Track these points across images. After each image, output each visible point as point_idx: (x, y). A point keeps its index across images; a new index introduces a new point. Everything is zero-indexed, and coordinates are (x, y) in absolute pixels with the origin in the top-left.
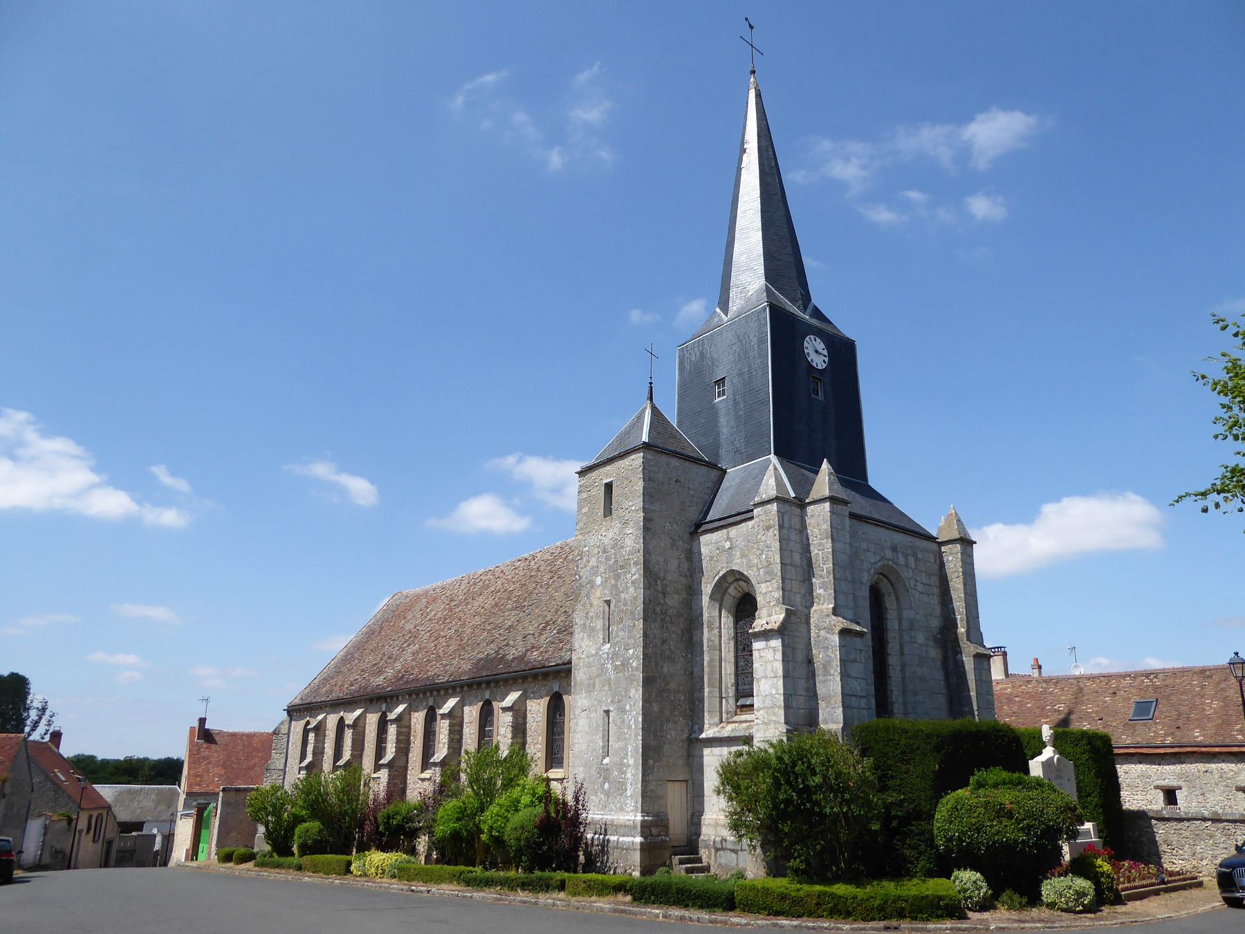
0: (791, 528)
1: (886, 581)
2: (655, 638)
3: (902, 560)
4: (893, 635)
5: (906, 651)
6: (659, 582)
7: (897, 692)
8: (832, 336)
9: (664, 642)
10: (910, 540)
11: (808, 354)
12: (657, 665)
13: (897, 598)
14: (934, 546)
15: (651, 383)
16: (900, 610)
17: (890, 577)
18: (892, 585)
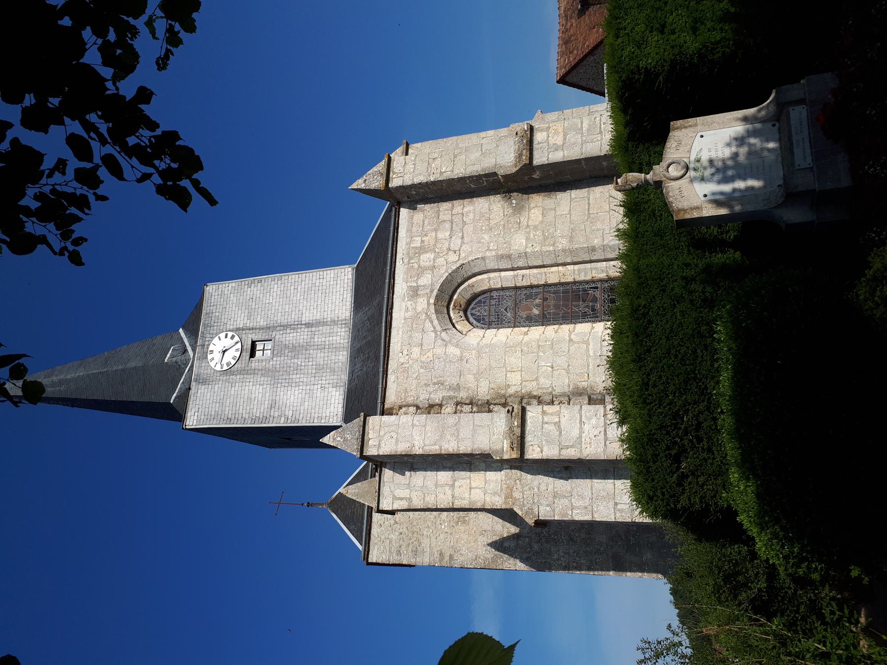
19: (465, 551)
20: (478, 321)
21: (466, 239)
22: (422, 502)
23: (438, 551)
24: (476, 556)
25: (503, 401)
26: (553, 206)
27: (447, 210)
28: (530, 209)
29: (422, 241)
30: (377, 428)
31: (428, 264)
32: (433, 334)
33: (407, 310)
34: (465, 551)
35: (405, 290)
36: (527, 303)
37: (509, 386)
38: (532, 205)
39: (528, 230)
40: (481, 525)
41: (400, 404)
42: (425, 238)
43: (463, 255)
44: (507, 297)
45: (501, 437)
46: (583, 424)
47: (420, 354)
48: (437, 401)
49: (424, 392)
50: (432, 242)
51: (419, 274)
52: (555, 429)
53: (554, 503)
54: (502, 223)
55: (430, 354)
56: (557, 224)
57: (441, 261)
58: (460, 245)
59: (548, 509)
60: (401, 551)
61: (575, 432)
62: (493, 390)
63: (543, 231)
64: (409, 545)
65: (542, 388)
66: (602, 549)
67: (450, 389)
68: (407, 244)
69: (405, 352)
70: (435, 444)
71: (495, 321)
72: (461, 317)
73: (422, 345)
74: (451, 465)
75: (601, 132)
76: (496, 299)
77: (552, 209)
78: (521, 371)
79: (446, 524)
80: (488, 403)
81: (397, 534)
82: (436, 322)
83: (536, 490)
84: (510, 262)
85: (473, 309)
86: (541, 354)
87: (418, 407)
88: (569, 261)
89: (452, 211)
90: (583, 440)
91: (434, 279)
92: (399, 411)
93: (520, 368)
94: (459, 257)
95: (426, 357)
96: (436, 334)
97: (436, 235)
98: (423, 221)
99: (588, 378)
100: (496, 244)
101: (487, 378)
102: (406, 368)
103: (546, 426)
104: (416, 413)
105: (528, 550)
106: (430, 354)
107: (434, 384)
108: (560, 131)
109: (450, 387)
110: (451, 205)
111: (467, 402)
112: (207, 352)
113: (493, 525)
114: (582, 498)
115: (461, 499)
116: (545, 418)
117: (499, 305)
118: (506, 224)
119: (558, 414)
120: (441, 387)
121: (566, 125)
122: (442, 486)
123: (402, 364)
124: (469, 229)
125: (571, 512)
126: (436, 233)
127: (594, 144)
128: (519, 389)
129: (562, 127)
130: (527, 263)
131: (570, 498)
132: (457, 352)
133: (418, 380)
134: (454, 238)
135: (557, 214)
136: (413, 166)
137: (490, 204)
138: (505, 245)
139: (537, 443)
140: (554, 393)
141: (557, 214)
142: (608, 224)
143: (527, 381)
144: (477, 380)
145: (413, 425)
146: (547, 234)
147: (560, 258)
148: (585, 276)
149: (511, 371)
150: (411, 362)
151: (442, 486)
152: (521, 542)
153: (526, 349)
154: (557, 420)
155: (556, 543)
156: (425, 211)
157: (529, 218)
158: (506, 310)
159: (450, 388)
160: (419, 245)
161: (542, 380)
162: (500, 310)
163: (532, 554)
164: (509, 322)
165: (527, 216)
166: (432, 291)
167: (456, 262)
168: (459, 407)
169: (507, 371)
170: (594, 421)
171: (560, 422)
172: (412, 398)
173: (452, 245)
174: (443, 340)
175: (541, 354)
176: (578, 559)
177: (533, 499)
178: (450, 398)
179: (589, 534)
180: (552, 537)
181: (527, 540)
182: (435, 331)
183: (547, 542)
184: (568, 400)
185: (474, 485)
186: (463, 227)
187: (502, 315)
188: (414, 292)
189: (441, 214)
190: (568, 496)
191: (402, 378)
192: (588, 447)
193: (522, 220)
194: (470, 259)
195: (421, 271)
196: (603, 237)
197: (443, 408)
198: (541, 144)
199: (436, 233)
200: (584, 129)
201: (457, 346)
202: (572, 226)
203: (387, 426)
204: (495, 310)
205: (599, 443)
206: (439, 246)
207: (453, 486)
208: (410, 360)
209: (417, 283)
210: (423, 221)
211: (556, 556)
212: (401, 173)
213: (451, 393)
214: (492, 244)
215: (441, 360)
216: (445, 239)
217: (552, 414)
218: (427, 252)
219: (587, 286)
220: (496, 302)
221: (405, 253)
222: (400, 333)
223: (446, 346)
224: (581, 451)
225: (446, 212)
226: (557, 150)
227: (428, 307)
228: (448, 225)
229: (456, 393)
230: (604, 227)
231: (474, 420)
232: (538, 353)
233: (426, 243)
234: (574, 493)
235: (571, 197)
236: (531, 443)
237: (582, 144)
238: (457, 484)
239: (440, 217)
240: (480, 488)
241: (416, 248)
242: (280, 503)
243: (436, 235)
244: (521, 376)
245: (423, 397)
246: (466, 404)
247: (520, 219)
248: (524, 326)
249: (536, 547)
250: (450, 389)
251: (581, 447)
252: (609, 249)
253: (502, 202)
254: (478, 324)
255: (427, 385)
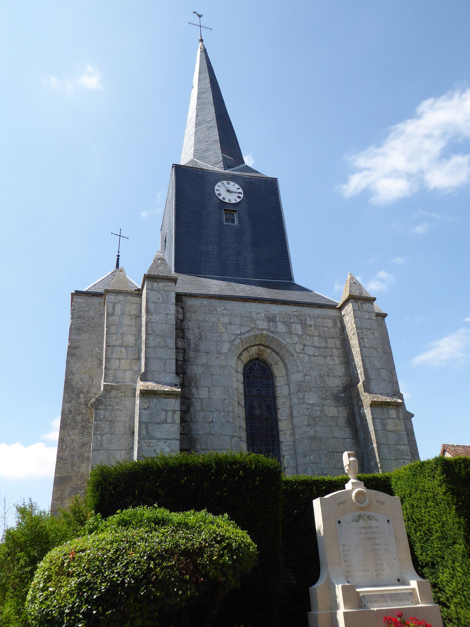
0: (124, 314)
1: (268, 351)
2: (73, 442)
3: (281, 328)
4: (283, 400)
5: (295, 414)
6: (82, 396)
7: (288, 457)
8: (250, 178)
9: (83, 445)
10: (294, 310)
11: (224, 198)
12: (73, 465)
13: (285, 365)
14: (333, 313)
15: (118, 256)
16: (287, 375)
17: (271, 346)
18: (278, 354)
19: (78, 365)
20: (250, 369)
21: (313, 359)
22: (111, 324)
23: (79, 345)
24: (74, 373)
25: (186, 384)
26: (339, 424)
27: (335, 344)
28: (336, 407)
29: (311, 325)
30: (166, 289)
31: (293, 329)
32: (239, 333)
33: (258, 314)
34: (78, 365)
35: (273, 312)
36: (264, 406)
37: (198, 389)
38: (339, 408)
39: (320, 405)
40: (97, 377)
41: (185, 308)
42: (313, 328)
43: (301, 356)
44: (269, 391)
45: (156, 380)
46: (165, 441)
47: (223, 323)
48: (187, 335)
49: (194, 326)
50: (310, 333)
51: (285, 323)
52: (161, 419)
53: (106, 421)
54: (326, 386)
55: (223, 330)
56: (325, 427)
57: (296, 339)
58: (308, 353)
59: (102, 416)
60: (80, 319)
61: (158, 435)
62: (194, 376)
63: (319, 417)
64: (84, 324)
65: (195, 413)
66: (75, 468)
67: (196, 344)
68: (308, 314)
69: (225, 312)
70: (152, 330)
71: (249, 381)
72: (253, 355)
73: (230, 324)
74: (137, 345)
75: (397, 459)
76: (267, 382)
77: (337, 423)
78: (209, 398)
79: (98, 351)
80: (184, 373)
81: (93, 316)
82: (248, 335)
83: (117, 407)
84: (295, 392)
85: (260, 365)
86: (223, 414)
87: (182, 321)
88: (296, 437)
89: (334, 348)
90: (152, 441)
91: (281, 334)
92: (180, 307)
93: (211, 397)
94: (299, 353)
95: (221, 327)
96: (239, 335)
97: (316, 336)
98: (326, 327)
99: (203, 450)
100: (309, 381)
101: (204, 372)
102: (212, 313)
103: (164, 413)
104: (178, 319)
105: (77, 412)
106: (223, 330)
107: (200, 333)
108: (397, 428)
109: (198, 345)
110: (339, 347)
111: (185, 357)
112: (228, 180)
113: (96, 386)
114: (109, 442)
115: (112, 352)
116: (170, 412)
117: (262, 384)
118: (325, 389)
119: (173, 422)
120: (197, 338)
121: (402, 432)
122: (122, 338)
123: (216, 309)
124: (321, 360)
125: (99, 433)
126: (318, 336)
127: (388, 454)
128: (195, 397)
129: (400, 430)
130: (294, 405)
131: (109, 433)
132: (225, 350)
133: (203, 321)
134: (314, 349)
135: (333, 428)
136: (367, 318)
137: (340, 377)
138: (309, 388)
139: (151, 406)
140: (192, 423)
141: (333, 428)
142: (325, 467)
143: (201, 403)
144: (202, 365)
145: (167, 315)
146: (317, 419)
147: (299, 430)
148: (285, 450)
149: (209, 391)
150: (217, 316)
151: (122, 338)
152: (83, 407)
153: (227, 402)
154: (169, 421)
155: (81, 433)
156: (334, 328)
157: (330, 406)
158: (259, 390)
159: (197, 345)
160: (308, 323)
161: (202, 414)
162: (258, 385)
163: (74, 415)
164: (249, 392)
165: (332, 405)
166: (272, 332)
167: (295, 351)
168: (182, 351)
169: (209, 387)
170: (167, 449)
171: (167, 423)
172: (189, 317)
173: (308, 348)
174: (234, 340)
175: (223, 414)
176: (69, 450)
177: (110, 405)
178: (189, 345)
179: (87, 459)
180: (86, 431)
181: (84, 411)
182: (241, 334)
183: (82, 427)
184: (186, 433)
185: (122, 361)
186: (323, 356)
187: (254, 387)
188: (271, 319)
189: (332, 340)
190: (111, 431)
191: (205, 309)
192: (147, 445)
193: (328, 401)
194: (298, 361)
195: (288, 325)
196: (315, 463)
197: (182, 340)
198: (386, 413)
199: (318, 336)
200: (399, 446)
201: (229, 350)
202: (324, 439)
203: (167, 295)
204: (258, 382)
205: (149, 453)
206: (308, 338)
207: (122, 346)
208: (218, 315)
209: (278, 321)
210: (326, 327)
211: (71, 433)
212: (362, 308)
213: (193, 345)
214: (309, 378)
215: (219, 339)
216: (313, 343)
217: (173, 417)
218: (302, 328)
219: (277, 452)
220: (265, 383)
221: (301, 313)
222: (240, 308)
223: (230, 342)
224: (144, 439)
225: (334, 344)
226: (382, 425)
227: (259, 329)
228: (323, 345)
229: (192, 349)
230: (323, 464)
231: (170, 359)
232: (223, 411)
233: (309, 328)
234: (113, 437)
235: (347, 438)
236: (151, 401)
237: (387, 445)
238: (123, 349)
239: (330, 339)
240: (119, 366)
241: (306, 321)
242: (120, 236)
243: (316, 336)
244: (205, 398)
245: (191, 325)
246: (184, 356)
247: (329, 399)
248: (245, 403)
249: (79, 418)
250: (196, 344)
251: (147, 439)
252: (306, 467)
253: (342, 385)
254: (247, 368)
255: (199, 327)
